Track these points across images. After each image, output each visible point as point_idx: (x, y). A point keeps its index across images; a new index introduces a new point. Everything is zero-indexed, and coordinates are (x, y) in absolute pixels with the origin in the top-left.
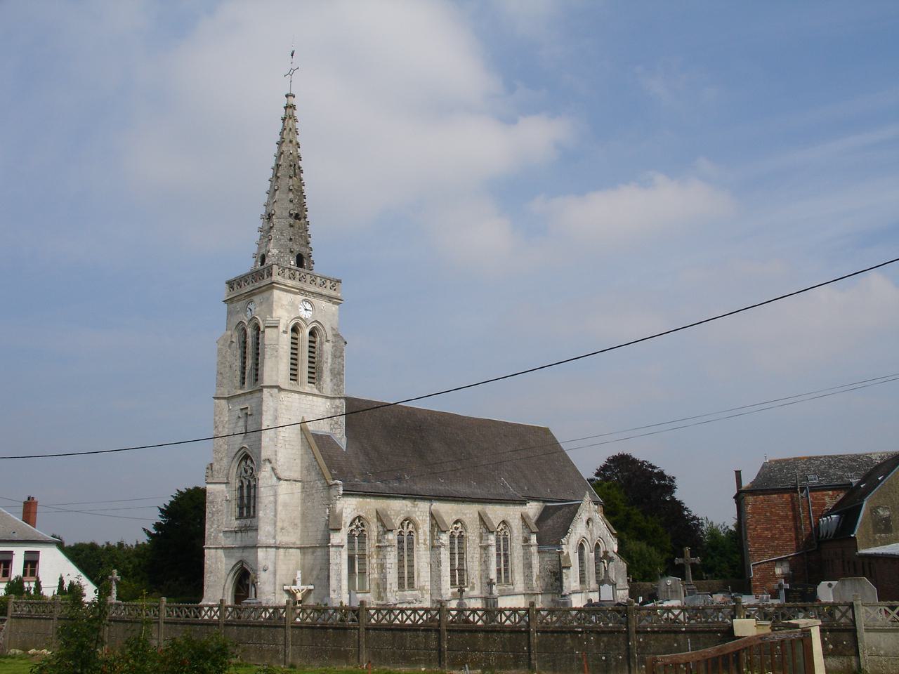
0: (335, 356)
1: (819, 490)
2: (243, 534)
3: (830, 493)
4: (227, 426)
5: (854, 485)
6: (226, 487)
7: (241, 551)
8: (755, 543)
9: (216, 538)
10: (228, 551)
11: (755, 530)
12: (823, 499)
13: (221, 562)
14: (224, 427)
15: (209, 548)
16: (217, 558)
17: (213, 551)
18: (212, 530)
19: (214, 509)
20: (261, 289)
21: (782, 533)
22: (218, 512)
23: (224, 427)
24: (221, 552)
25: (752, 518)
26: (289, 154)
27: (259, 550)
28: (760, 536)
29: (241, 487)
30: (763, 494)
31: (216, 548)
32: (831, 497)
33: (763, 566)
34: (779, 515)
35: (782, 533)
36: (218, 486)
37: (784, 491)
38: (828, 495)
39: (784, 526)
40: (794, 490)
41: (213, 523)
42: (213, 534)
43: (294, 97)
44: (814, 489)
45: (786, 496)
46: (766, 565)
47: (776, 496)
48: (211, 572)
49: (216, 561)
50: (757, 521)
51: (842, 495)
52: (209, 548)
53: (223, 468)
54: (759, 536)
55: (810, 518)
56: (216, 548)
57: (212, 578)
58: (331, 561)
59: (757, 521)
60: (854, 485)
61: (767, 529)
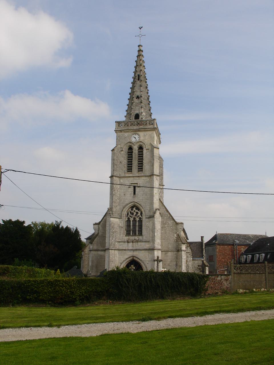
0: (160, 166)
1: (240, 246)
2: (134, 244)
3: (243, 247)
4: (119, 190)
5: (251, 245)
6: (119, 220)
7: (132, 251)
8: (219, 263)
9: (114, 245)
10: (120, 251)
11: (219, 258)
12: (241, 249)
13: (117, 257)
14: (118, 191)
15: (112, 249)
16: (115, 255)
17: (113, 251)
18: (113, 240)
19: (114, 231)
20: (146, 129)
21: (228, 260)
22: (115, 232)
23: (118, 191)
24: (116, 252)
25: (218, 254)
26: (144, 72)
27: (155, 251)
28: (221, 261)
29: (129, 221)
30: (222, 245)
31: (115, 250)
32: (243, 248)
33: (221, 272)
34: (227, 253)
35: (228, 260)
36: (115, 219)
37: (229, 245)
38: (242, 247)
39: (228, 257)
40: (233, 245)
41: (113, 237)
42: (113, 243)
43: (142, 46)
44: (239, 245)
45: (230, 247)
46: (222, 272)
47: (226, 246)
48: (112, 262)
49: (114, 256)
50: (220, 255)
51: (247, 248)
52: (112, 249)
53: (117, 211)
54: (220, 261)
55: (237, 255)
56: (115, 250)
57: (113, 264)
58: (183, 258)
59: (220, 255)
60: (251, 245)
61: (223, 258)
